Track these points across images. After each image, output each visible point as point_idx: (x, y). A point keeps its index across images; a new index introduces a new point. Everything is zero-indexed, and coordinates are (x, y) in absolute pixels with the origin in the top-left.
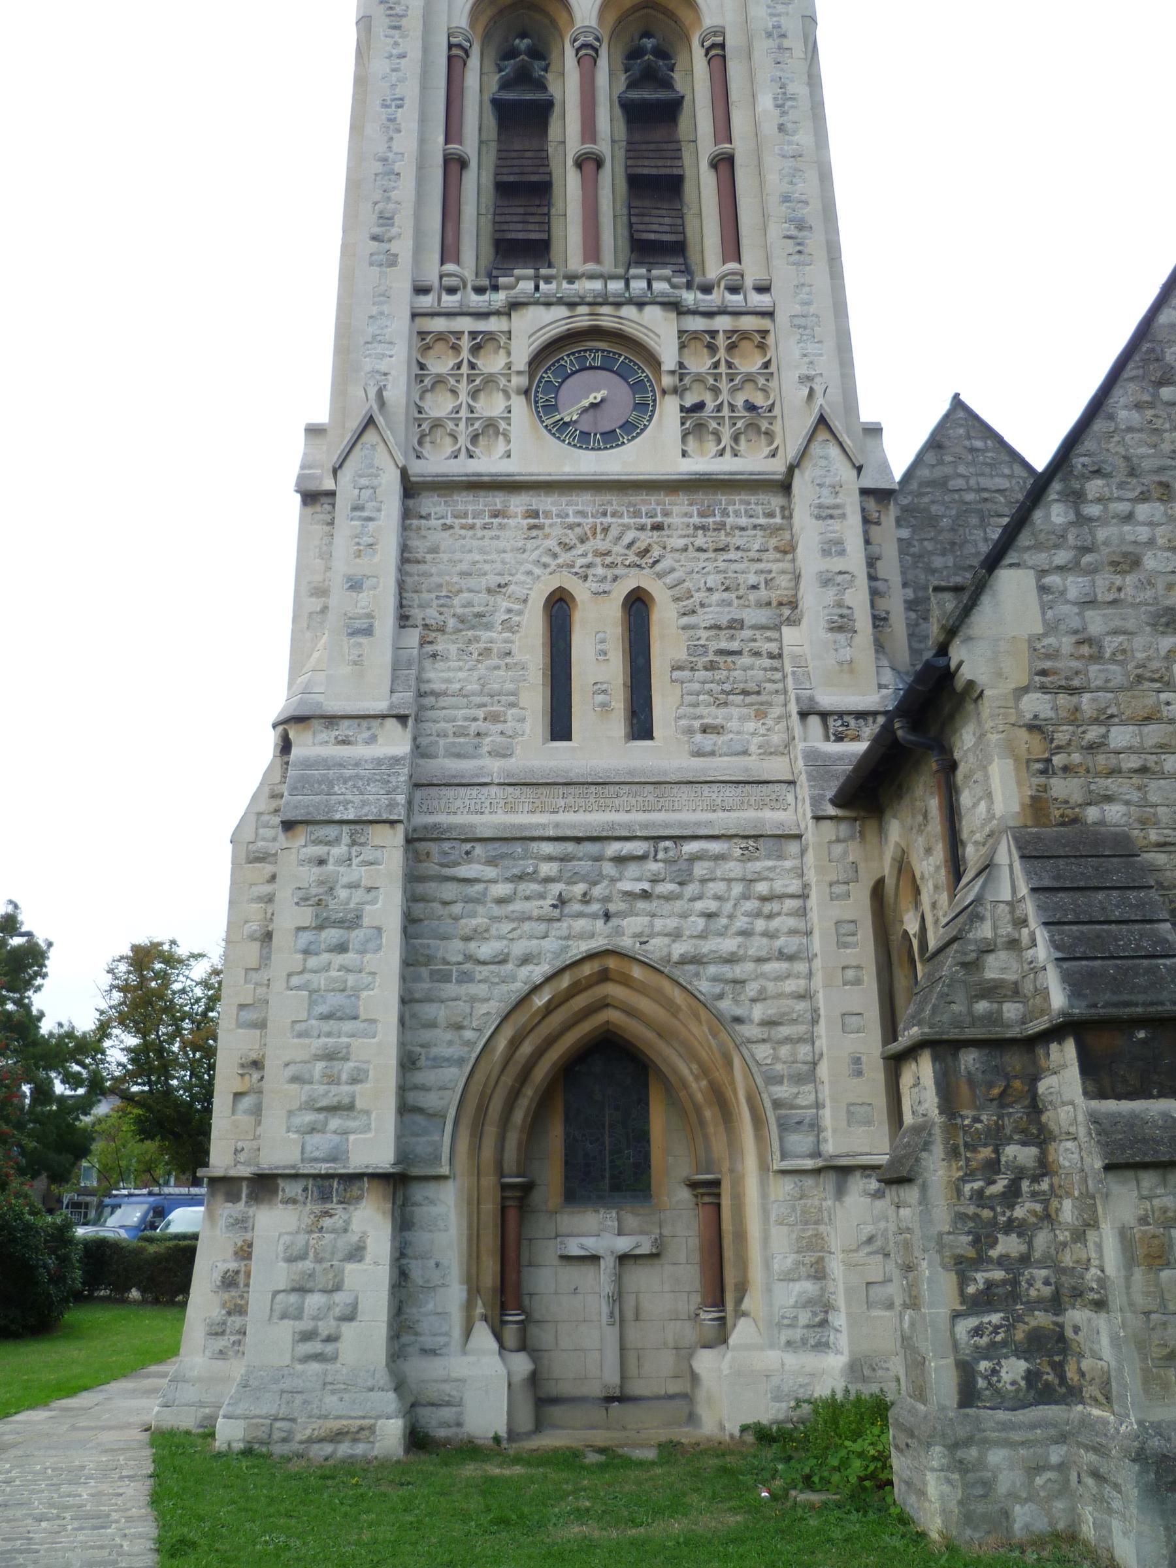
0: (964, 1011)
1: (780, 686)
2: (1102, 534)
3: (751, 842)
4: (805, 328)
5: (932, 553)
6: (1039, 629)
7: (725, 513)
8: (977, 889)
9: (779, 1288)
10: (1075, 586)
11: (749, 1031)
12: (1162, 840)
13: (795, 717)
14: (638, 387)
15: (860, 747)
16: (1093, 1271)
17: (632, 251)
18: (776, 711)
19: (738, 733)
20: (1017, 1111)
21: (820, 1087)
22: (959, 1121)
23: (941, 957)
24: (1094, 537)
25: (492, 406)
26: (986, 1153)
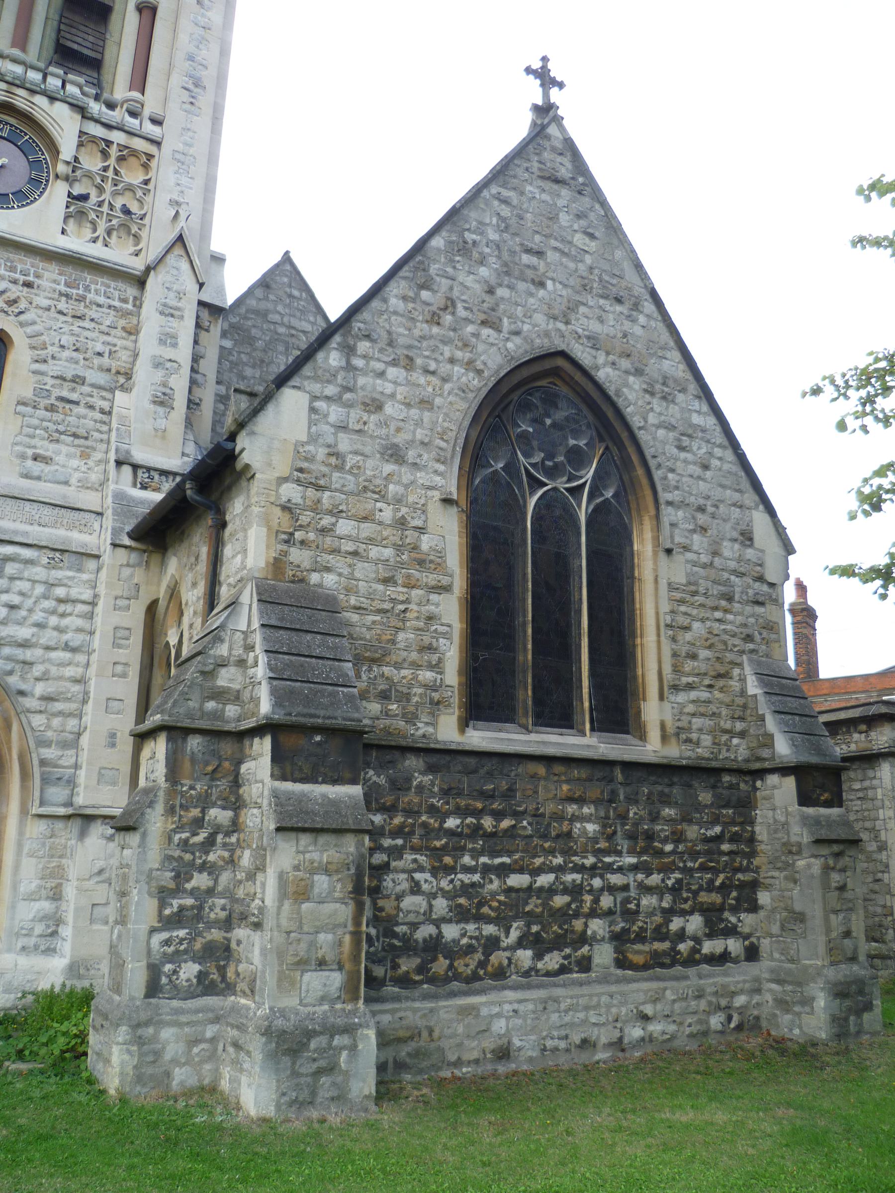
0: (194, 707)
1: (105, 437)
2: (361, 381)
3: (58, 554)
4: (183, 163)
5: (246, 364)
6: (304, 438)
7: (87, 289)
8: (223, 618)
9: (22, 906)
10: (335, 413)
11: (29, 703)
12: (358, 604)
13: (112, 464)
14: (36, 165)
15: (158, 497)
16: (257, 901)
17: (56, 52)
18: (98, 456)
19: (64, 466)
20: (223, 784)
21: (80, 753)
22: (179, 787)
23: (187, 665)
24: (355, 382)
26: (195, 812)
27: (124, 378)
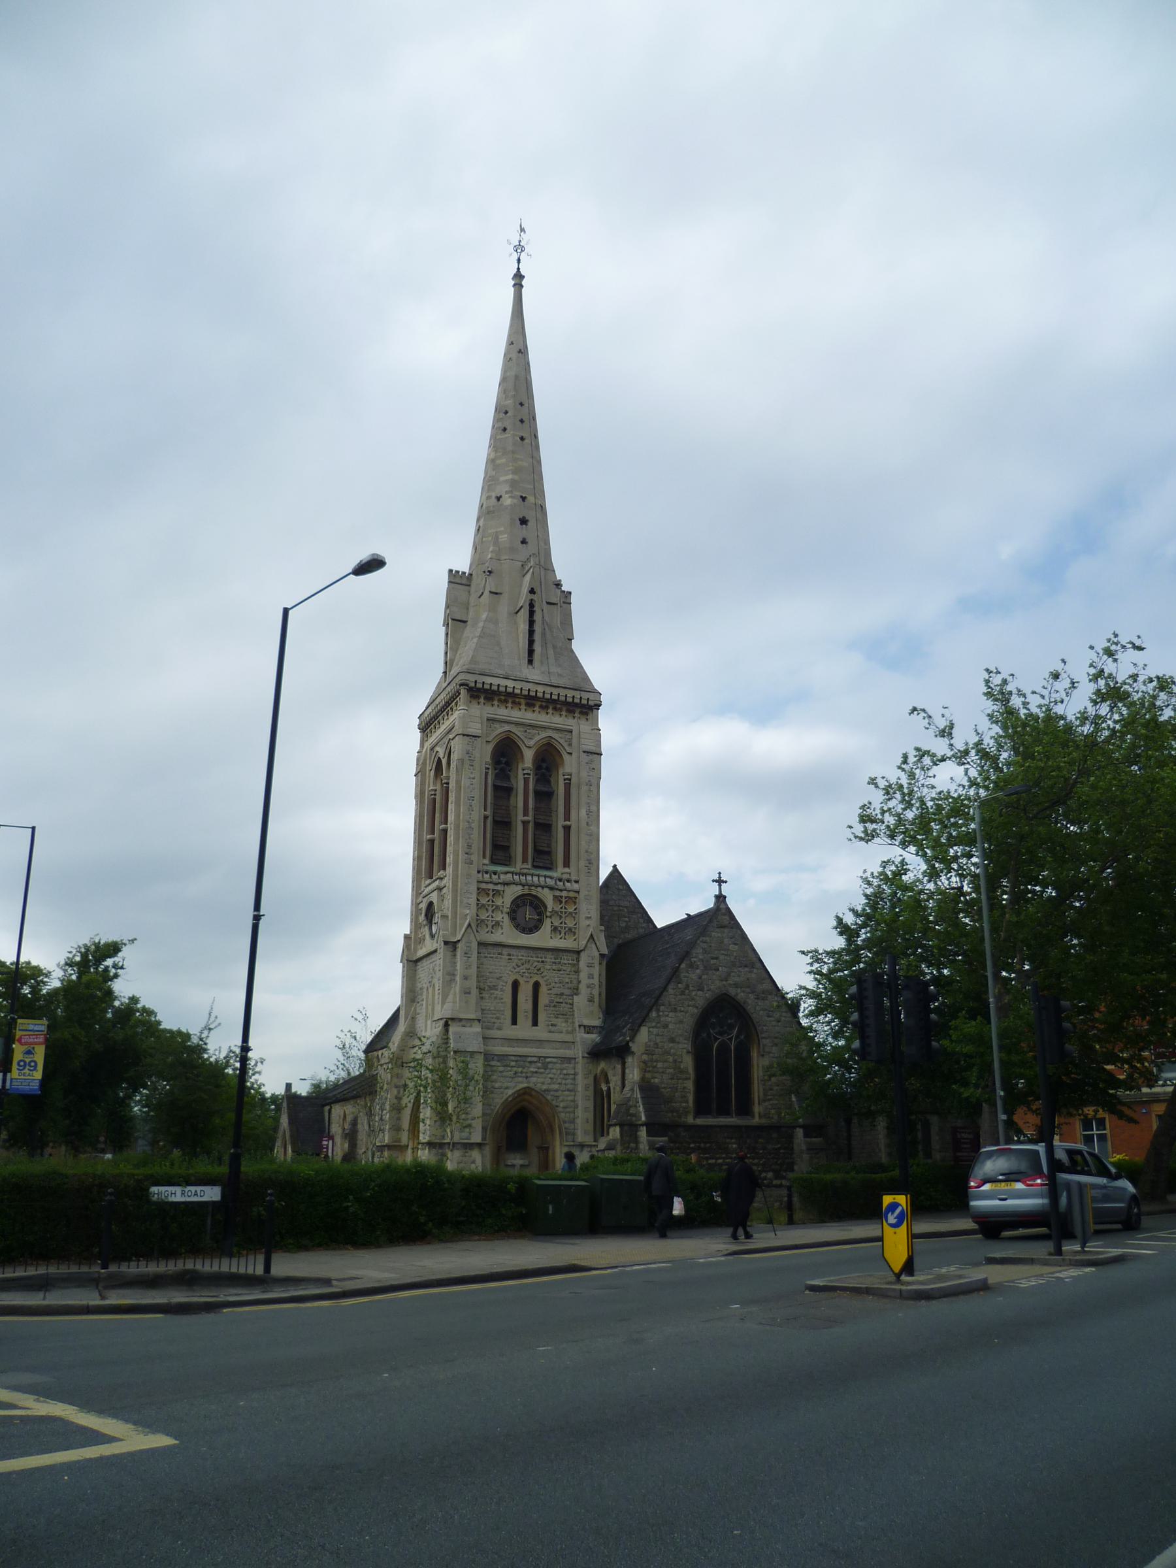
10: (655, 1031)
25: (498, 917)
27: (576, 991)
